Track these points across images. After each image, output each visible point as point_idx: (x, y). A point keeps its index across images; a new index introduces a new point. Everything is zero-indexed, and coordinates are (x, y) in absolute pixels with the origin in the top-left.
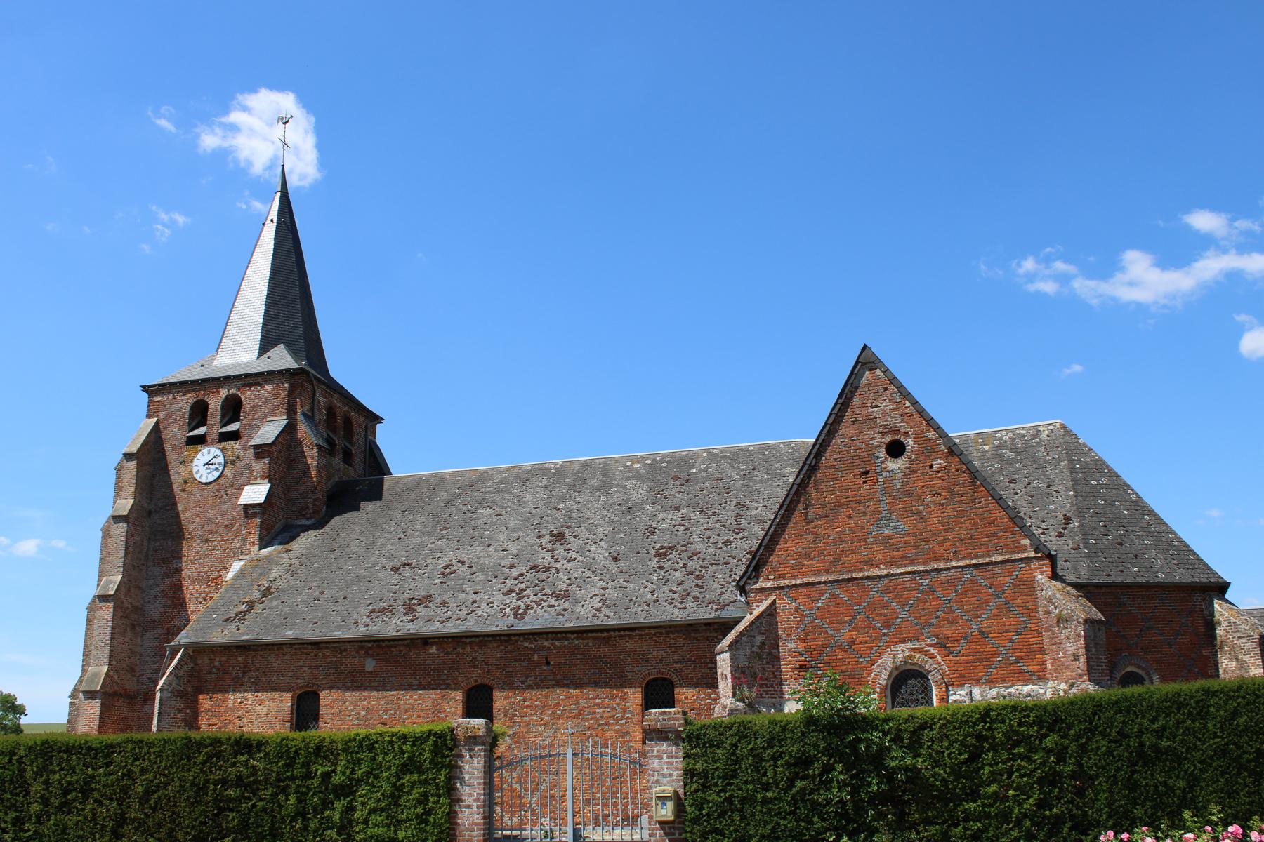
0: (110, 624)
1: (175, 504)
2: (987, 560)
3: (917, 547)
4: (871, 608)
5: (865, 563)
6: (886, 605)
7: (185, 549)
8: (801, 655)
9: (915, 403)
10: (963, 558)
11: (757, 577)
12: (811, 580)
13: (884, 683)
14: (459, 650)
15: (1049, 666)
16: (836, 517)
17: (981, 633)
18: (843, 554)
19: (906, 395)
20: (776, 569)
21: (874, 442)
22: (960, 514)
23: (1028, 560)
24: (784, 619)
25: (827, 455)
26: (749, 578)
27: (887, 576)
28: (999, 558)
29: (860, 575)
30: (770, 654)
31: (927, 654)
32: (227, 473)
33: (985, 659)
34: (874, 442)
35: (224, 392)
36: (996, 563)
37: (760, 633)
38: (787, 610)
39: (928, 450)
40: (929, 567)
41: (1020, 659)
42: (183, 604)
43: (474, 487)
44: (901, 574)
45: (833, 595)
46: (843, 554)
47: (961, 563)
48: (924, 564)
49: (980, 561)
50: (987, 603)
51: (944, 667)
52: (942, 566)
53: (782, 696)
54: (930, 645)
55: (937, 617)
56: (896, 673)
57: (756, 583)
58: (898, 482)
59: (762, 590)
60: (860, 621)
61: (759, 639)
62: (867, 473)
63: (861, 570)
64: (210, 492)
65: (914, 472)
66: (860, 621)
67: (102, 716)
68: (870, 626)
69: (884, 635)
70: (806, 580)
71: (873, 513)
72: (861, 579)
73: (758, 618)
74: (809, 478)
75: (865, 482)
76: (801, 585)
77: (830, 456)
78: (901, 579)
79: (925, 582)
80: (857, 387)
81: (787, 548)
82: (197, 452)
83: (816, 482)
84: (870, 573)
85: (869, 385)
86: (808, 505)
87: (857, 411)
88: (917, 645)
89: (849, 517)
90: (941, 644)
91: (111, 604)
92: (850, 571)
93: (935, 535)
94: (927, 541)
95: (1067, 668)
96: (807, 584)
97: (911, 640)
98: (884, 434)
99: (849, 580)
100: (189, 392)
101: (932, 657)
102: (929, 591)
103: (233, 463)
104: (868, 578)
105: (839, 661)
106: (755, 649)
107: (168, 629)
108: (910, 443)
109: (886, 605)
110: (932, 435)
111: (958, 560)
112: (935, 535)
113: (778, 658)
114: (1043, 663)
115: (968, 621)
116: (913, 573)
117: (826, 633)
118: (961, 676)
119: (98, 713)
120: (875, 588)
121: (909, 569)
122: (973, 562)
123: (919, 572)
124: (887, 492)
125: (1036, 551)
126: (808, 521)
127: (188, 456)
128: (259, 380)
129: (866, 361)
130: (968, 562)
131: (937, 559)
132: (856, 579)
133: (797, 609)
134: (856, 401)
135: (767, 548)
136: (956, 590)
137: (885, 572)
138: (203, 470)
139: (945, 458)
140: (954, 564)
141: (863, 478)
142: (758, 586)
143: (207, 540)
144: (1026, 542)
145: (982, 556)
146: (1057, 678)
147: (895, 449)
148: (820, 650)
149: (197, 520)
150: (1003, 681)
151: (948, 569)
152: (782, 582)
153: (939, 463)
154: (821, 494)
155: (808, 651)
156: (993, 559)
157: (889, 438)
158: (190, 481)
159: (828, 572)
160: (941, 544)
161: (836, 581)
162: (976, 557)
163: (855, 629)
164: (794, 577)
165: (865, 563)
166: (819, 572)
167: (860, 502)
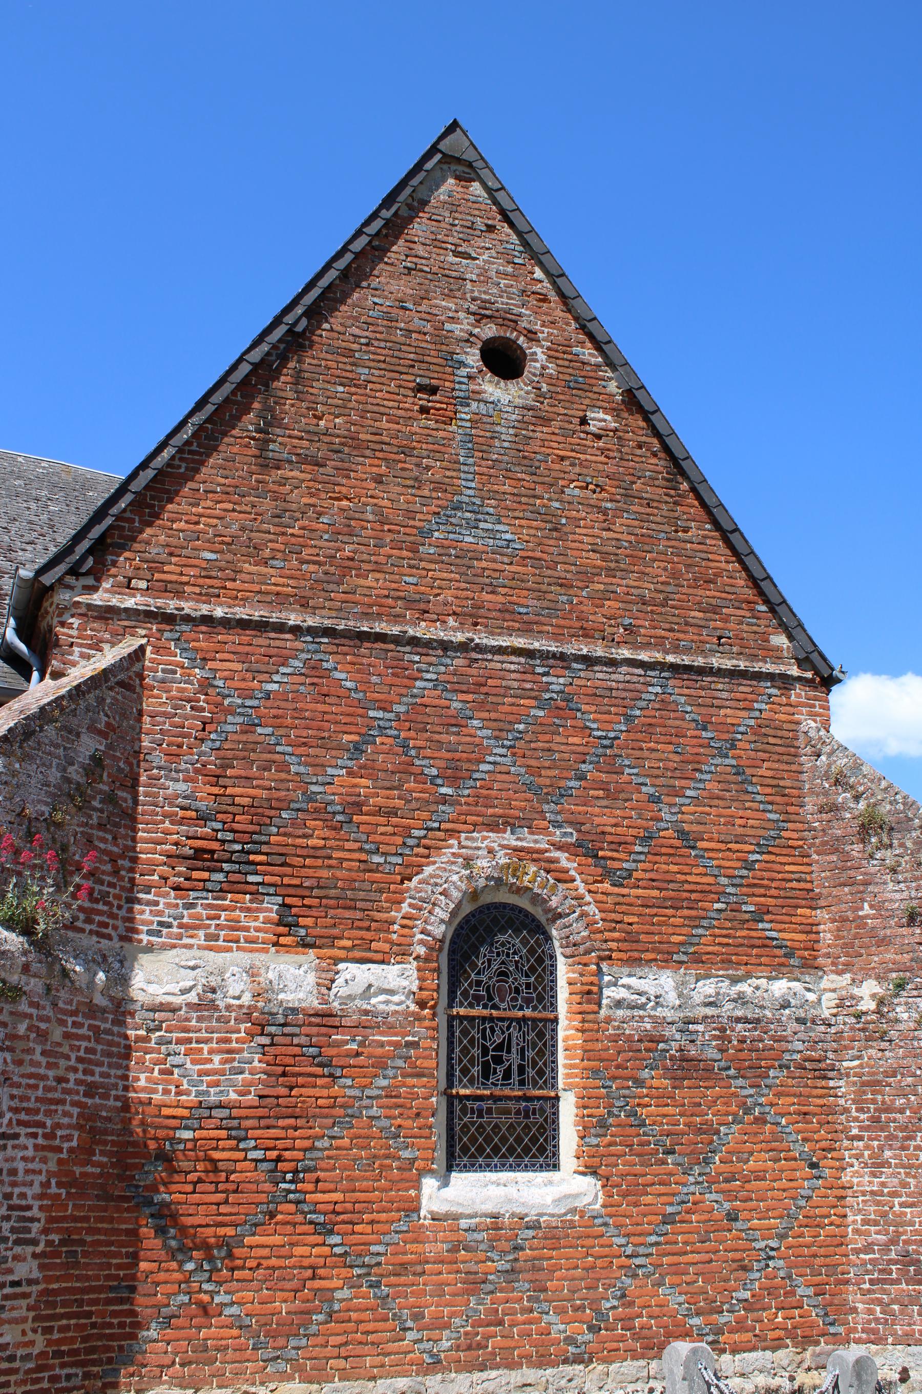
2: (700, 661)
3: (541, 595)
4: (416, 719)
5: (410, 603)
6: (457, 723)
8: (203, 818)
9: (555, 276)
10: (646, 646)
11: (98, 574)
12: (257, 615)
13: (439, 930)
15: (827, 937)
16: (346, 472)
17: (683, 834)
18: (349, 566)
19: (535, 254)
20: (156, 566)
21: (459, 329)
22: (644, 542)
23: (785, 682)
24: (166, 702)
25: (335, 321)
26: (74, 571)
27: (464, 647)
28: (728, 664)
29: (395, 630)
30: (110, 799)
31: (550, 866)
33: (685, 900)
34: (459, 329)
36: (720, 672)
37: (92, 729)
38: (174, 679)
39: (576, 384)
40: (571, 648)
41: (760, 915)
43: (364, 249)
44: (501, 650)
45: (314, 669)
46: (349, 566)
47: (644, 656)
48: (556, 637)
49: (687, 660)
50: (696, 763)
51: (592, 909)
52: (600, 652)
53: (128, 934)
54: (560, 847)
55: (581, 777)
56: (467, 909)
57: (94, 589)
58: (507, 433)
59: (107, 614)
60: (381, 754)
61: (89, 745)
62: (433, 390)
63: (397, 618)
65: (546, 421)
66: (381, 754)
68: (407, 769)
69: (444, 800)
70: (241, 613)
71: (439, 486)
72: (397, 640)
73: (78, 692)
74: (284, 359)
75: (424, 410)
76: (226, 623)
77: (341, 324)
78: (496, 663)
79: (558, 682)
80: (424, 203)
81: (198, 515)
83: (298, 378)
84: (420, 631)
85: (453, 207)
86: (270, 423)
87: (421, 250)
88: (528, 840)
89: (378, 480)
90: (586, 849)
92: (366, 615)
93: (587, 576)
94: (564, 585)
95: (884, 942)
96: (244, 624)
97: (510, 823)
98: (480, 318)
99: (363, 637)
101: (563, 878)
102: (565, 706)
104: (414, 641)
105: (314, 853)
106: (74, 772)
108: (538, 357)
109: (457, 723)
110: (588, 353)
111: (636, 646)
112: (587, 576)
113: (131, 819)
114: (811, 929)
115: (654, 800)
116: (529, 654)
117: (284, 767)
118: (631, 938)
120: (430, 672)
121: (520, 642)
122: (670, 658)
123: (545, 656)
124: (479, 446)
125: (802, 663)
126: (266, 463)
129: (449, 157)
130: (659, 656)
131: (586, 634)
132: (381, 637)
133: (206, 685)
134: (419, 228)
135: (139, 504)
136: (629, 719)
137: (460, 637)
139: (615, 412)
140: (625, 653)
141: (423, 399)
142: (98, 599)
144: (780, 640)
145: (687, 651)
146: (848, 967)
147: (503, 360)
148: (262, 813)
150: (727, 962)
151: (613, 663)
152: (171, 605)
153: (600, 419)
154: (315, 403)
155: (225, 807)
156: (716, 662)
157: (489, 331)
159: (304, 605)
160: (599, 599)
161: (329, 632)
162: (676, 650)
163: (369, 770)
164: (207, 597)
165: (410, 603)
166: (281, 600)
167: (407, 451)
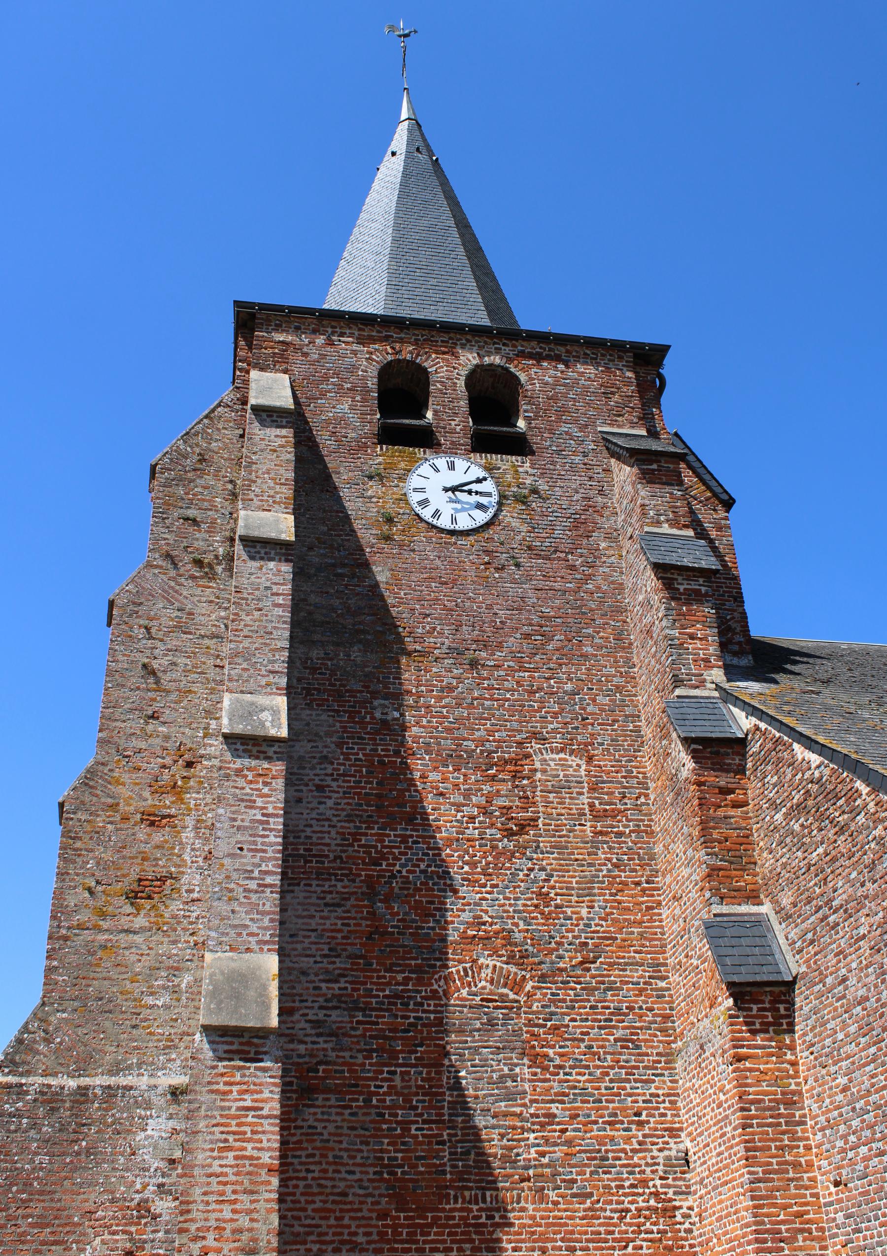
0: (277, 824)
1: (366, 565)
7: (408, 676)
14: (471, 1092)
32: (509, 516)
35: (469, 359)
42: (416, 818)
64: (467, 554)
67: (288, 1120)
82: (414, 462)
91: (278, 767)
100: (373, 340)
103: (522, 500)
107: (370, 883)
119: (273, 1107)
127: (390, 466)
128: (561, 350)
138: (439, 500)
143: (474, 664)
149: (438, 611)
158: (403, 523)
